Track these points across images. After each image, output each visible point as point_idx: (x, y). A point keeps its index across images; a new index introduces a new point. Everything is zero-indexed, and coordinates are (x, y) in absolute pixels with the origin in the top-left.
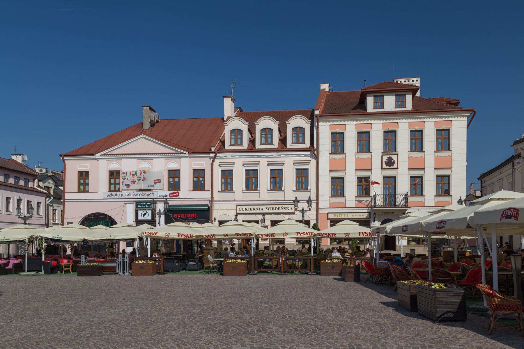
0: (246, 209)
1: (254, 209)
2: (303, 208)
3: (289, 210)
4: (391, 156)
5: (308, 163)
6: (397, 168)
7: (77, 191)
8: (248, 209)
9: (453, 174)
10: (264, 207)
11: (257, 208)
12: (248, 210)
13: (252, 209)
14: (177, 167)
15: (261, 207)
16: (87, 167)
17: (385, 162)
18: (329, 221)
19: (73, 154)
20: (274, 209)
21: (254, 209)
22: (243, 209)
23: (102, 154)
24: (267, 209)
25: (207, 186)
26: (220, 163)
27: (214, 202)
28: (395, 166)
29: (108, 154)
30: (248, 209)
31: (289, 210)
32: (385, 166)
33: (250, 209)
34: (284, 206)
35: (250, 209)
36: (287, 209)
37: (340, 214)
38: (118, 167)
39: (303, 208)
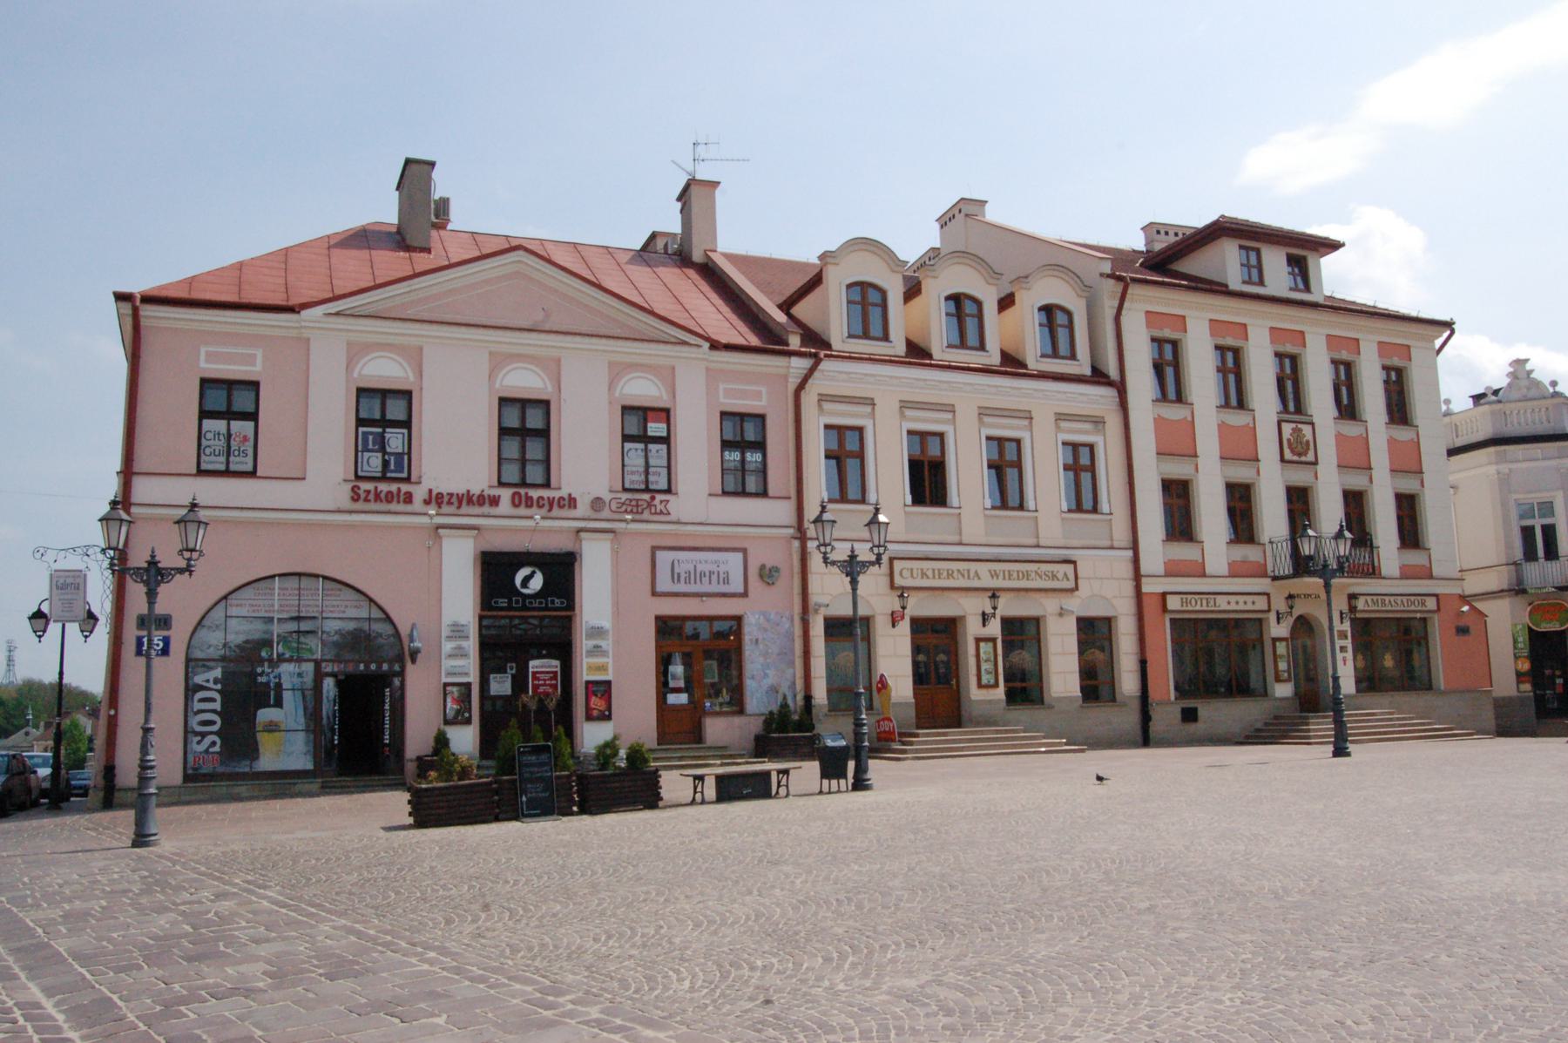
0: (924, 575)
1: (1026, 575)
2: (153, 556)
3: (1058, 580)
4: (1300, 426)
5: (1098, 422)
6: (1315, 463)
7: (194, 471)
8: (930, 573)
9: (1201, 476)
10: (983, 568)
11: (959, 571)
12: (931, 576)
13: (945, 574)
14: (407, 378)
15: (973, 566)
16: (251, 360)
17: (1289, 440)
18: (1167, 617)
19: (510, 325)
20: (1015, 575)
21: (1026, 575)
22: (915, 571)
23: (333, 311)
24: (994, 575)
25: (780, 476)
26: (982, 411)
27: (183, 529)
28: (1310, 457)
29: (348, 312)
30: (930, 573)
31: (1058, 580)
32: (1288, 455)
33: (1007, 573)
34: (1044, 567)
35: (1007, 573)
36: (1054, 577)
37: (1197, 597)
38: (401, 374)
39: (153, 556)
